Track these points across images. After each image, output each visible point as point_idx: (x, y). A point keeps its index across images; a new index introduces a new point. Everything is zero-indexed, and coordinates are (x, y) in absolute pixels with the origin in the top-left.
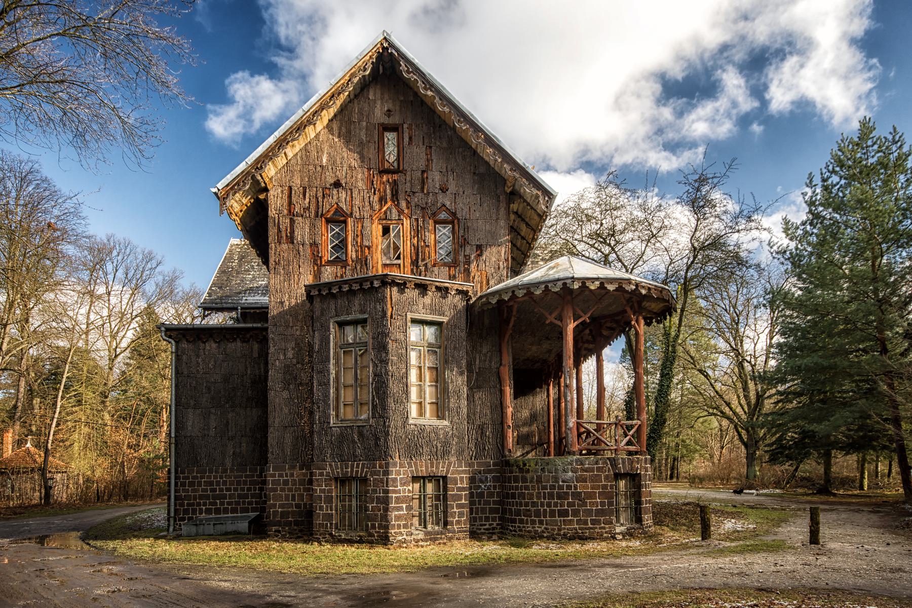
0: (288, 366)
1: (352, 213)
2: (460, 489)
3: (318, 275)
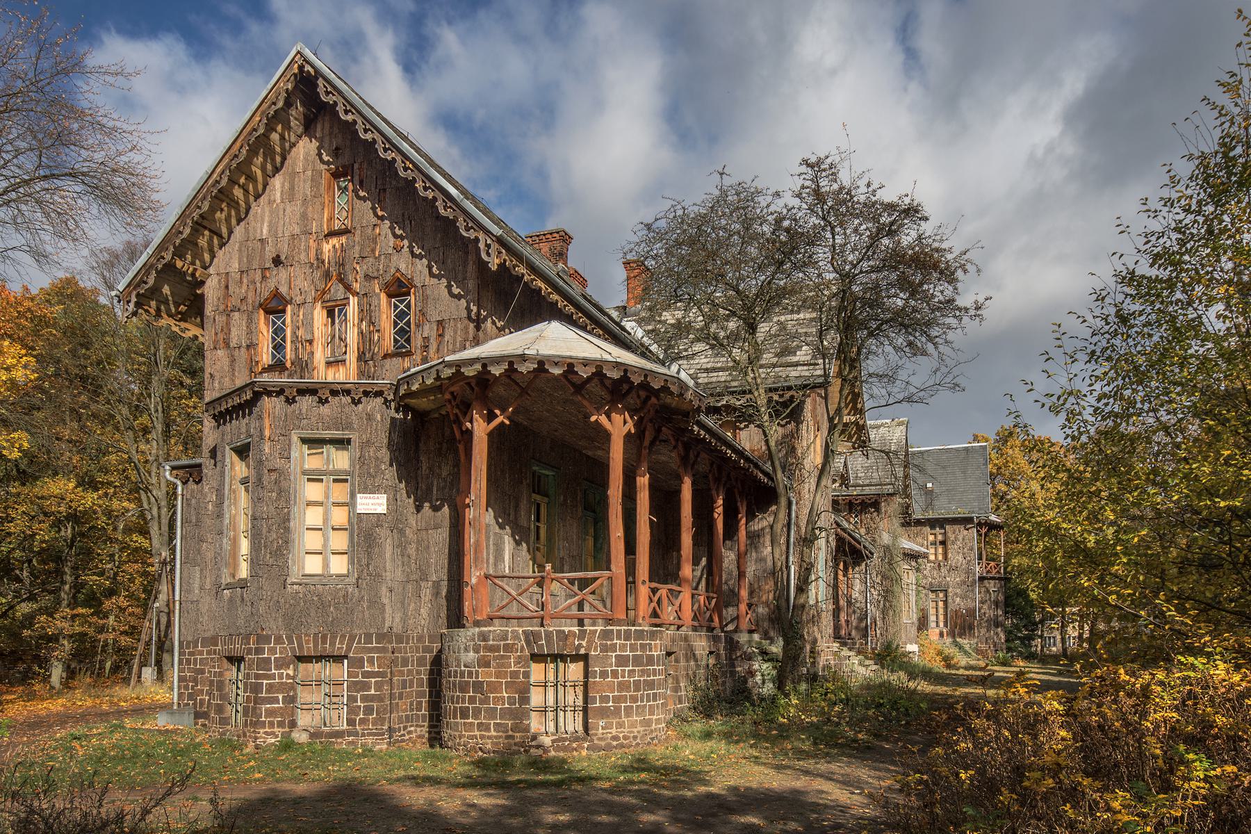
2: (367, 675)
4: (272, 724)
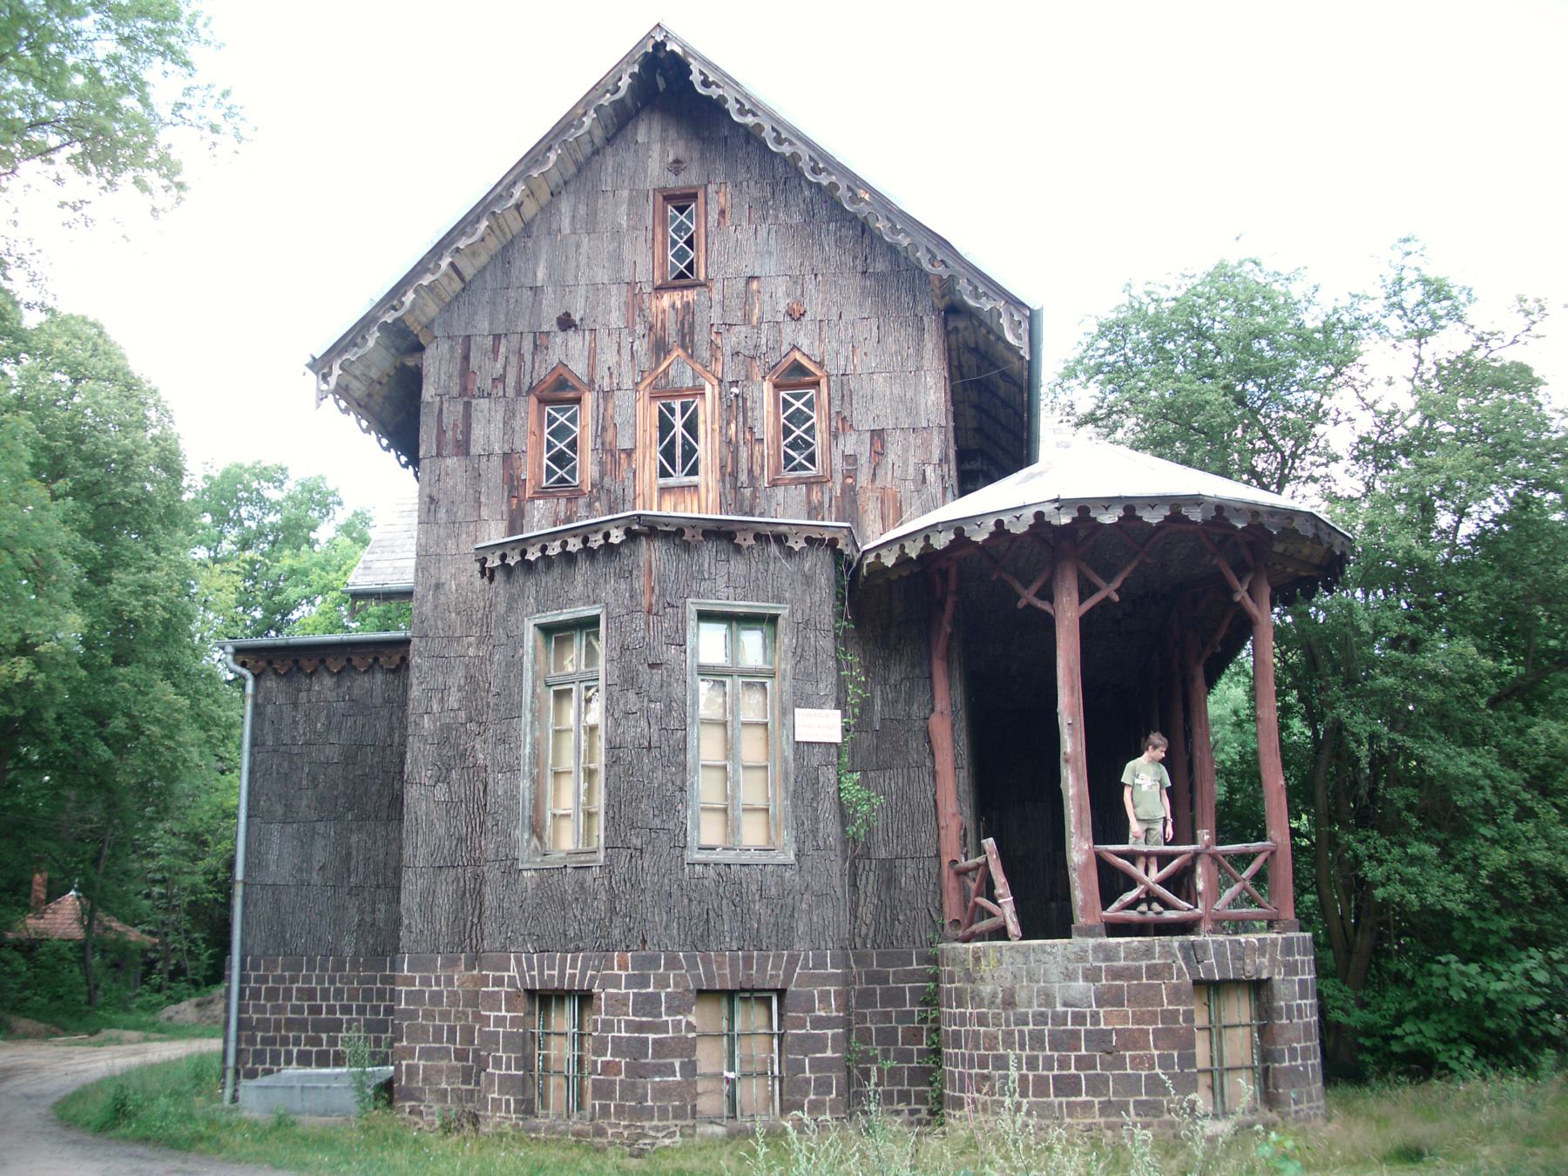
0: (448, 727)
1: (592, 381)
2: (819, 1023)
3: (515, 520)
4: (663, 1113)
